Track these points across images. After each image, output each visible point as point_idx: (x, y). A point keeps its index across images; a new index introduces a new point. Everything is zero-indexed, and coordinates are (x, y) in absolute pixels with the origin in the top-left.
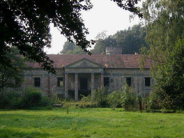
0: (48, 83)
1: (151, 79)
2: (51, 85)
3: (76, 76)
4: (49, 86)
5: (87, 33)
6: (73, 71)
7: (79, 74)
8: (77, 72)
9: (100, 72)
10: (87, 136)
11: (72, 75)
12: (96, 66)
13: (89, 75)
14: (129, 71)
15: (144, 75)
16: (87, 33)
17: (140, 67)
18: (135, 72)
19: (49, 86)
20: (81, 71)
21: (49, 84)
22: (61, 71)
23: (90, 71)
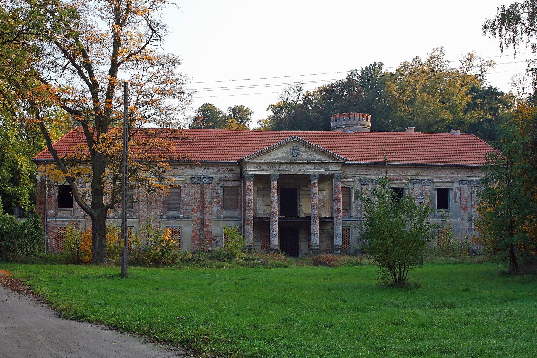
0: (200, 201)
1: (451, 192)
2: (208, 205)
3: (275, 183)
4: (202, 207)
5: (498, 9)
6: (265, 171)
7: (282, 178)
8: (275, 172)
9: (330, 173)
10: (444, 351)
11: (262, 181)
12: (324, 159)
13: (306, 179)
14: (399, 171)
15: (433, 182)
16: (498, 9)
17: (116, 174)
18: (412, 174)
19: (202, 207)
20: (285, 170)
21: (204, 204)
22: (232, 170)
23: (308, 169)
